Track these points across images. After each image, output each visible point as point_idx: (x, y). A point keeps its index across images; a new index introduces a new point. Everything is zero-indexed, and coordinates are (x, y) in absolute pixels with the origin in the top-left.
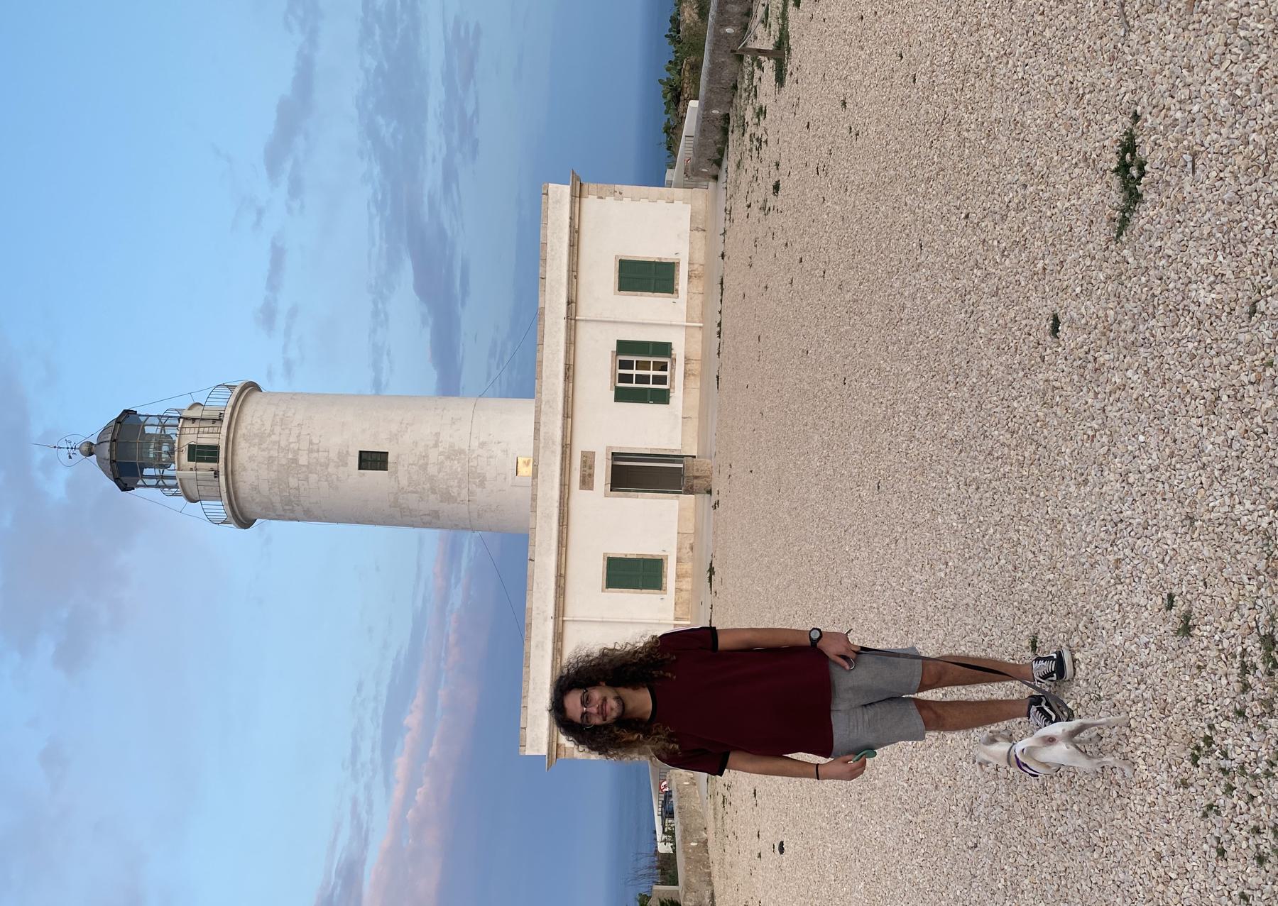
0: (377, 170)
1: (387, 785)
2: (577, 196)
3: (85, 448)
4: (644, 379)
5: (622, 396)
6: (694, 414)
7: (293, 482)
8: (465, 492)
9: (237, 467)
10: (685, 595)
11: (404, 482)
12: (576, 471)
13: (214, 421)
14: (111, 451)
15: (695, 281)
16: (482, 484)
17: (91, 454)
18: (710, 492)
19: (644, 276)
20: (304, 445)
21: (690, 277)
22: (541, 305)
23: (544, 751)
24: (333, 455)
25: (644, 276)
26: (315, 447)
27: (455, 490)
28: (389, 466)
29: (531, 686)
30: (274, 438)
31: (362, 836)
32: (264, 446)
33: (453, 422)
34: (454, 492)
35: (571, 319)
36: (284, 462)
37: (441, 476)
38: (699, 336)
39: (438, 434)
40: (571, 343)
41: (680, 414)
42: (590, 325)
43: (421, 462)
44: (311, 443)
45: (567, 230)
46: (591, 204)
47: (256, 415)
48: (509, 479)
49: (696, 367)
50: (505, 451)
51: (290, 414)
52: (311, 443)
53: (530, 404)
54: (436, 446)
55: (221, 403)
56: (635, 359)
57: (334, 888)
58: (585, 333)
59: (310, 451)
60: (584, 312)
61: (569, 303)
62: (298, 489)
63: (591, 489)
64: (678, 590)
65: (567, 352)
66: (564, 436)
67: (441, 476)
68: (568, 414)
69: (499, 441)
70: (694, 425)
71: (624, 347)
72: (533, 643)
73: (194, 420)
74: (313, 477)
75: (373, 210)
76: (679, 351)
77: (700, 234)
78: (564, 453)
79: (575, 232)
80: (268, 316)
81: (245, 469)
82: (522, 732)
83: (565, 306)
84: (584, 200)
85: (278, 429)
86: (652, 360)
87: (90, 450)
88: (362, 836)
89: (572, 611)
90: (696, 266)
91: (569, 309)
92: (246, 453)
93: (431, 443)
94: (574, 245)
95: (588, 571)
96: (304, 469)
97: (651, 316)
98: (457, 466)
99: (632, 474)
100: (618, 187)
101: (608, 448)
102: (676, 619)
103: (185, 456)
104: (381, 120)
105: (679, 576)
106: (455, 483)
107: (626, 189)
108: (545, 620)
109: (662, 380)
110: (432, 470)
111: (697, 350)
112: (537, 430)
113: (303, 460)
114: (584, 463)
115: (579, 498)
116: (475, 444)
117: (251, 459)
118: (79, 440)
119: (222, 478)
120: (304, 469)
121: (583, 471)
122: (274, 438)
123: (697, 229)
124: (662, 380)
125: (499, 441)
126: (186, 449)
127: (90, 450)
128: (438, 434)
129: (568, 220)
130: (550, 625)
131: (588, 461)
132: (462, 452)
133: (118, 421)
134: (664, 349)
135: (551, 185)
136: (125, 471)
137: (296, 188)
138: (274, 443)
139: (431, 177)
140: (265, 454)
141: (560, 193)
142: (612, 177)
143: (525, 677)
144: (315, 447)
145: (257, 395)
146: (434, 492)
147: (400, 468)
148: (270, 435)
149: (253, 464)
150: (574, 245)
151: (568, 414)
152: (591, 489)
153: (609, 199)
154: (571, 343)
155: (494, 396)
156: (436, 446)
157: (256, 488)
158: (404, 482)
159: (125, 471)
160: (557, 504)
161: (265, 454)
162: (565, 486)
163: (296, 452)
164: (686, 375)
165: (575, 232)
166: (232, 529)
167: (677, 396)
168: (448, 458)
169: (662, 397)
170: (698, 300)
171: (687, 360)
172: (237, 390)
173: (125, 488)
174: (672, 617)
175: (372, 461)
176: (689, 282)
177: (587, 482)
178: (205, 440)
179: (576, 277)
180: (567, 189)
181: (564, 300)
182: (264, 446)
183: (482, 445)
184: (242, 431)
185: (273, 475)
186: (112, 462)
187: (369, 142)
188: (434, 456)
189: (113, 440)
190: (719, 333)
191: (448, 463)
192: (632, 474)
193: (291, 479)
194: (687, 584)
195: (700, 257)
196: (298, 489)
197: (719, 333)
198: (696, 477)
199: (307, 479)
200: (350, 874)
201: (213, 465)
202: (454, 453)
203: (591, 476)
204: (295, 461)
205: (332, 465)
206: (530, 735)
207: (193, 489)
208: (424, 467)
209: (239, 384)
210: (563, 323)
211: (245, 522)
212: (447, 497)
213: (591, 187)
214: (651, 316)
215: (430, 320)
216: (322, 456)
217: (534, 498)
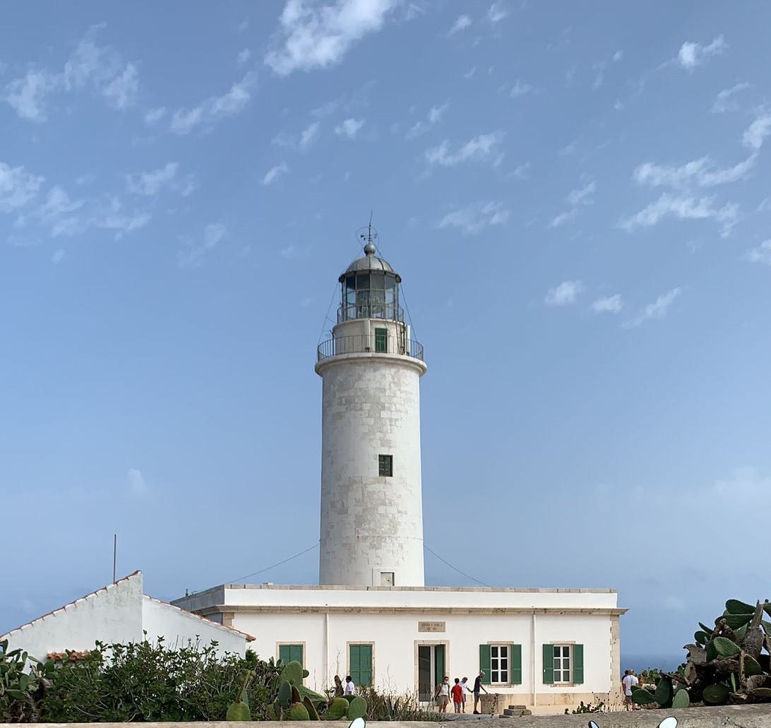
2: (613, 614)
4: (504, 664)
7: (367, 407)
11: (370, 488)
16: (373, 546)
21: (565, 694)
23: (227, 603)
26: (393, 423)
27: (367, 526)
35: (534, 612)
37: (378, 515)
43: (387, 501)
44: (396, 420)
46: (606, 624)
52: (396, 420)
53: (423, 585)
54: (399, 512)
71: (579, 649)
74: (372, 421)
85: (403, 395)
89: (333, 622)
91: (541, 609)
95: (361, 631)
96: (377, 415)
100: (618, 640)
101: (448, 641)
107: (618, 646)
112: (411, 589)
113: (384, 414)
114: (437, 624)
115: (413, 623)
121: (432, 623)
126: (383, 326)
128: (406, 513)
131: (439, 627)
134: (579, 679)
136: (355, 280)
141: (609, 601)
144: (393, 423)
147: (382, 485)
153: (610, 636)
156: (399, 512)
157: (360, 378)
158: (370, 488)
159: (355, 280)
162: (423, 611)
163: (389, 409)
167: (549, 689)
168: (391, 521)
175: (386, 465)
177: (424, 627)
181: (545, 607)
182: (392, 385)
185: (372, 392)
191: (387, 521)
193: (369, 405)
196: (361, 409)
201: (373, 347)
202: (394, 526)
203: (429, 630)
205: (381, 435)
208: (384, 504)
212: (359, 521)
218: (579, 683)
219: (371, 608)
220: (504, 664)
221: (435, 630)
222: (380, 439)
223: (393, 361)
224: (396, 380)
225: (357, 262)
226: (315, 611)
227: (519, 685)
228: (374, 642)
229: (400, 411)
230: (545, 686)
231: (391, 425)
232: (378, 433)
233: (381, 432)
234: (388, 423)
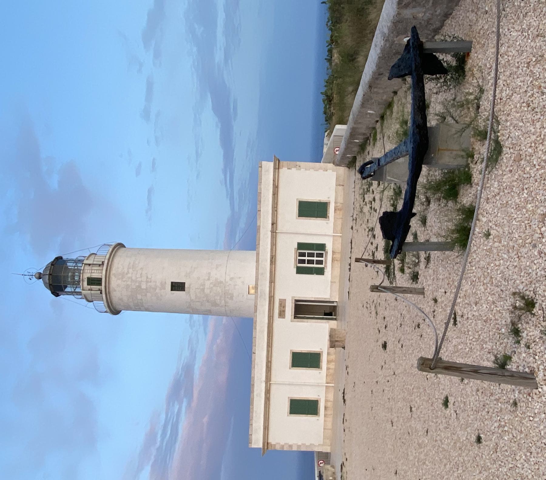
0: (195, 49)
1: (206, 333)
2: (277, 168)
3: (37, 276)
5: (300, 271)
6: (337, 280)
7: (139, 297)
8: (223, 301)
9: (111, 289)
10: (331, 371)
12: (276, 310)
13: (100, 265)
14: (49, 279)
15: (338, 212)
16: (232, 298)
17: (40, 278)
18: (344, 348)
19: (312, 210)
20: (144, 279)
21: (335, 210)
22: (258, 224)
23: (261, 446)
24: (158, 284)
25: (312, 210)
26: (150, 281)
28: (186, 289)
29: (254, 415)
30: (129, 275)
31: (193, 353)
32: (124, 279)
33: (217, 267)
34: (218, 302)
36: (134, 287)
38: (340, 240)
39: (209, 273)
40: (274, 244)
41: (330, 281)
42: (282, 235)
43: (201, 287)
44: (147, 278)
45: (272, 186)
46: (284, 172)
47: (121, 262)
48: (245, 296)
49: (338, 256)
50: (243, 282)
51: (137, 263)
52: (147, 278)
53: (255, 252)
55: (105, 253)
56: (307, 252)
57: (181, 374)
58: (281, 239)
59: (147, 282)
60: (280, 228)
61: (273, 224)
62: (141, 300)
63: (284, 318)
64: (328, 369)
65: (272, 249)
66: (270, 292)
67: (211, 294)
68: (272, 281)
69: (240, 274)
70: (337, 286)
71: (301, 246)
72: (255, 394)
73: (89, 265)
74: (149, 295)
75: (193, 69)
76: (329, 248)
77: (341, 188)
78: (270, 301)
79: (276, 187)
80: (146, 114)
81: (115, 291)
82: (250, 436)
83: (270, 225)
84: (281, 170)
85: (131, 271)
86: (315, 252)
87: (40, 276)
88: (193, 353)
89: (274, 378)
90: (338, 204)
91: (272, 227)
92: (114, 282)
93: (207, 278)
94: (275, 194)
97: (316, 230)
98: (219, 289)
99: (303, 310)
100: (298, 163)
102: (327, 383)
103: (85, 283)
104: (196, 26)
105: (329, 362)
106: (219, 298)
107: (302, 164)
108: (261, 382)
109: (320, 262)
110: (207, 291)
111: (339, 247)
113: (144, 286)
114: (280, 305)
115: (277, 322)
116: (228, 279)
117: (118, 286)
118: (34, 271)
119: (104, 296)
120: (144, 291)
122: (129, 275)
123: (340, 185)
124: (320, 262)
125: (240, 274)
127: (40, 276)
129: (272, 181)
130: (263, 385)
131: (282, 303)
132: (221, 282)
133: (52, 264)
134: (322, 247)
135: (263, 162)
137: (157, 55)
138: (129, 278)
139: (219, 56)
140: (125, 283)
141: (268, 166)
142: (295, 157)
143: (251, 410)
145: (123, 249)
146: (208, 301)
148: (127, 274)
149: (119, 287)
150: (275, 194)
151: (272, 281)
152: (284, 318)
154: (274, 244)
155: (239, 249)
156: (209, 279)
157: (121, 299)
158: (193, 297)
159: (57, 288)
160: (266, 326)
161: (125, 283)
164: (333, 260)
165: (276, 187)
166: (109, 315)
167: (328, 271)
168: (214, 285)
169: (320, 272)
170: (339, 222)
171: (333, 252)
172: (113, 247)
173: (57, 295)
174: (324, 380)
175: (178, 287)
176: (335, 212)
177: (282, 314)
178: (95, 275)
179: (276, 211)
180: (272, 164)
181: (270, 222)
182: (124, 279)
183: (232, 279)
184: (113, 271)
186: (50, 285)
187: (191, 36)
188: (208, 284)
189: (50, 274)
190: (350, 269)
191: (214, 288)
192: (303, 310)
194: (332, 366)
195: (341, 200)
196: (141, 300)
197: (350, 269)
198: (337, 341)
199: (146, 295)
200: (188, 370)
202: (218, 283)
203: (284, 311)
204: (139, 287)
206: (254, 437)
207: (90, 298)
208: (203, 290)
209: (114, 244)
210: (269, 234)
211: (115, 312)
212: (215, 304)
213: (283, 163)
214: (316, 230)
215: (219, 125)
216: (152, 284)
217: (256, 307)
218: (325, 247)
219: (266, 376)
220: (310, 262)
221: (284, 307)
222: (161, 289)
223: (109, 268)
224: (120, 277)
225: (45, 283)
226: (268, 392)
227: (326, 246)
228: (291, 350)
229: (141, 274)
230: (325, 273)
231: (151, 282)
232: (157, 291)
233: (156, 289)
234: (149, 284)
